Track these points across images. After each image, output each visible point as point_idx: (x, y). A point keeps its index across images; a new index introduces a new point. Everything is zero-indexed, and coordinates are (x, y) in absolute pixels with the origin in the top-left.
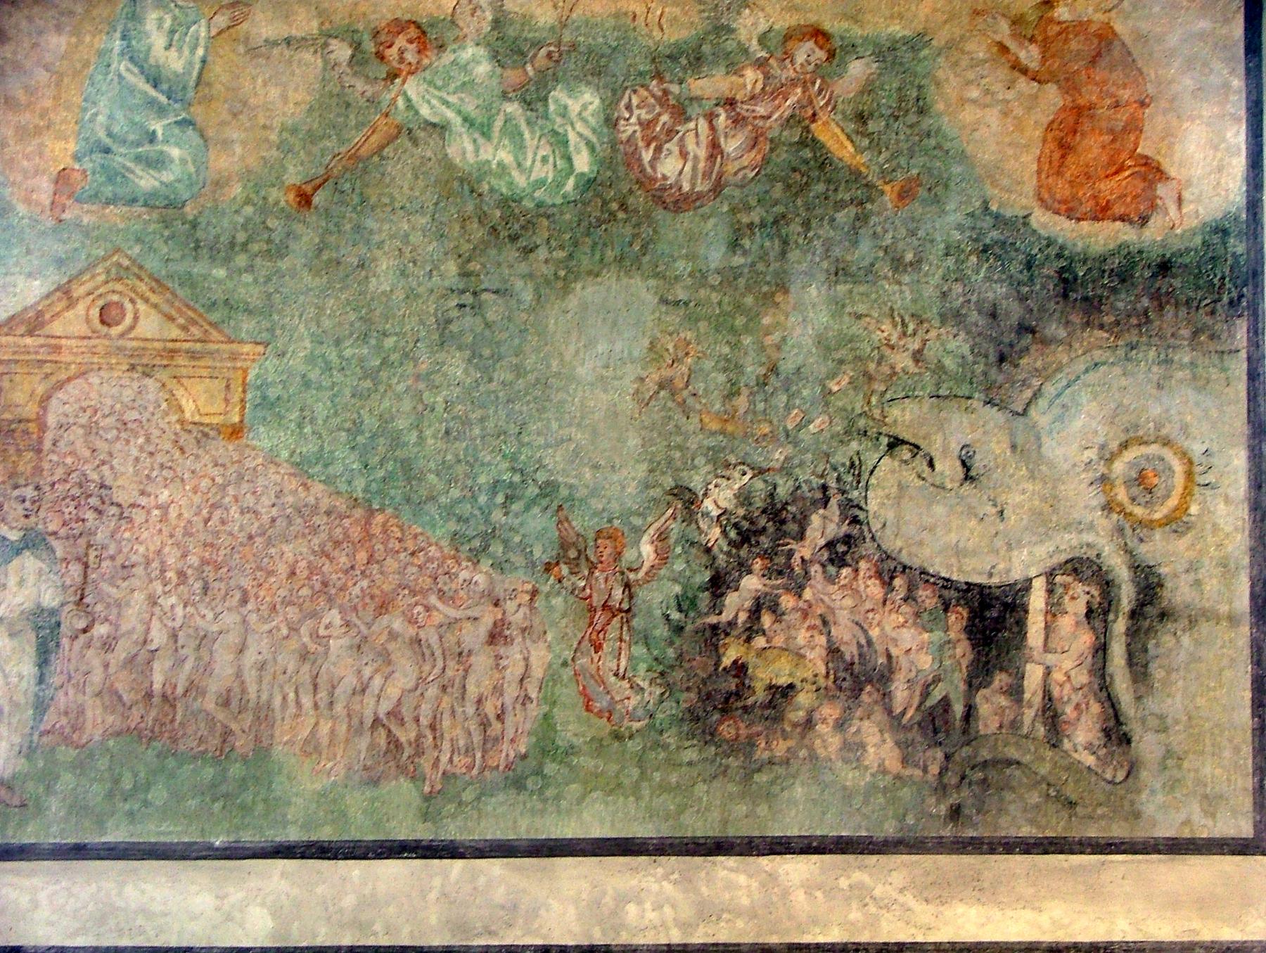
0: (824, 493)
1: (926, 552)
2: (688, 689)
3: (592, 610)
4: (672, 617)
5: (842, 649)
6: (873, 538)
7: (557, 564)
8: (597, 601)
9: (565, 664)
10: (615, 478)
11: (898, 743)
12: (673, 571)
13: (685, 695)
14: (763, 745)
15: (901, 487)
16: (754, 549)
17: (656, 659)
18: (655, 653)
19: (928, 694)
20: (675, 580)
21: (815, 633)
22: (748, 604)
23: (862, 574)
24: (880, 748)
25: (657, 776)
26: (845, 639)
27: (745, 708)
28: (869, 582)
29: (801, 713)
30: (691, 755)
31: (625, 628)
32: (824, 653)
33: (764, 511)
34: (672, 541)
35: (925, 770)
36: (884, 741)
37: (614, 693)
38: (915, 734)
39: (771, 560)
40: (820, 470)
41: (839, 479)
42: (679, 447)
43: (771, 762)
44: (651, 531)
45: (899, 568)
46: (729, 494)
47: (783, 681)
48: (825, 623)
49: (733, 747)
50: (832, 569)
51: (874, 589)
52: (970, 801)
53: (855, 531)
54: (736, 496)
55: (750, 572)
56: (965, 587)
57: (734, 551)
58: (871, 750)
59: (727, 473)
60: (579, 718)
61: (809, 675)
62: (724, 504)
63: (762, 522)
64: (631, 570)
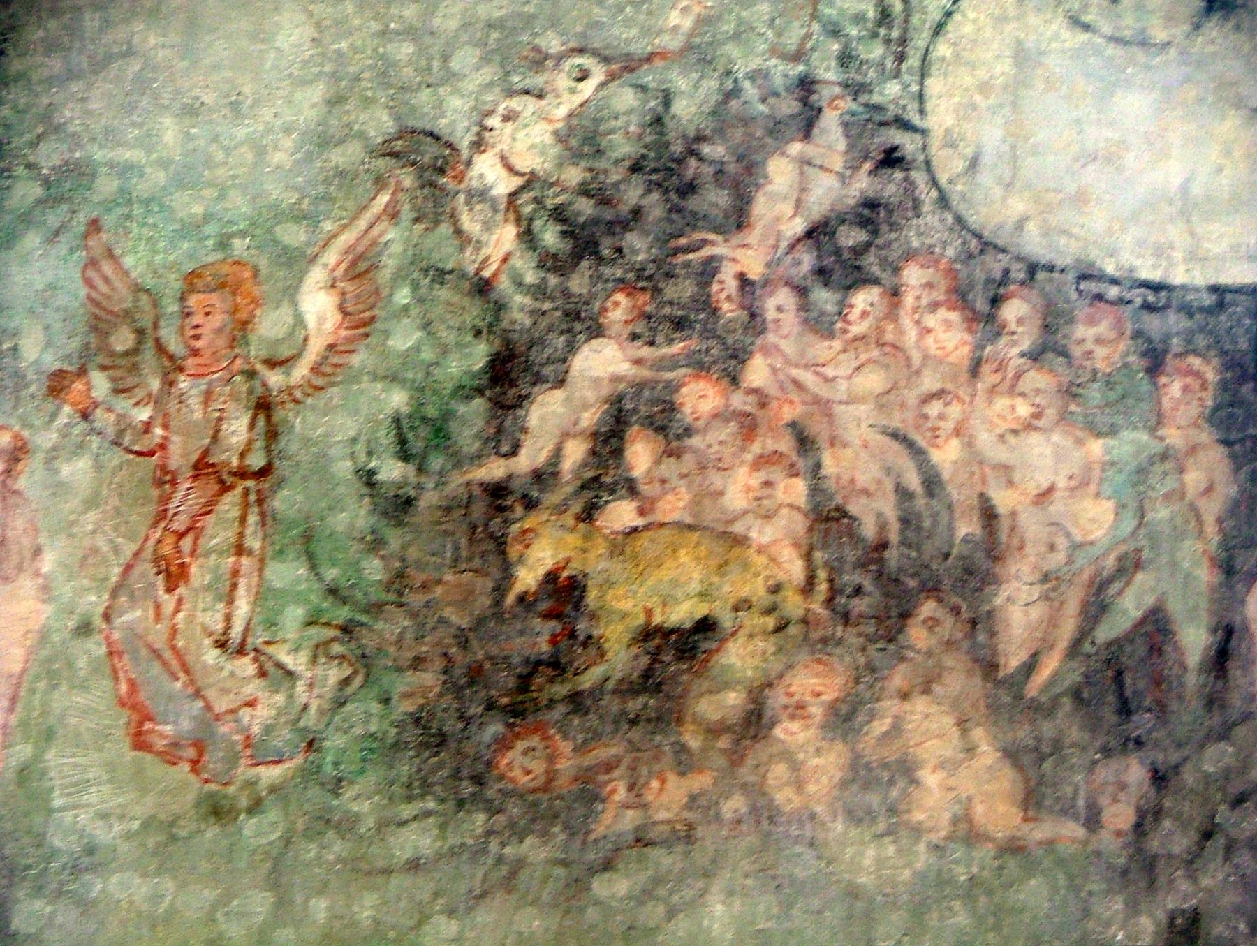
0: (805, 102)
1: (1096, 221)
2: (418, 663)
3: (166, 479)
4: (381, 477)
5: (853, 509)
6: (943, 201)
7: (82, 372)
8: (180, 455)
9: (84, 629)
10: (241, 133)
11: (1011, 754)
12: (385, 354)
13: (412, 679)
14: (621, 794)
15: (1022, 57)
16: (607, 271)
17: (333, 591)
18: (331, 574)
19: (1104, 608)
20: (393, 378)
21: (777, 474)
22: (588, 419)
23: (909, 300)
24: (955, 769)
25: (320, 908)
26: (863, 480)
27: (577, 701)
28: (931, 321)
29: (734, 699)
30: (417, 840)
31: (253, 519)
32: (800, 524)
33: (636, 168)
34: (384, 275)
35: (1093, 821)
36: (970, 750)
37: (211, 694)
38: (1067, 725)
39: (657, 291)
40: (791, 41)
41: (845, 59)
42: (410, 33)
43: (642, 840)
44: (331, 257)
45: (1018, 273)
46: (541, 133)
47: (682, 613)
48: (804, 442)
49: (545, 809)
50: (824, 297)
51: (948, 336)
52: (1231, 898)
53: (890, 187)
54: (560, 138)
55: (597, 332)
56: (1208, 300)
57: (553, 280)
58: (931, 779)
59: (538, 80)
60: (111, 767)
61: (756, 589)
62: (526, 162)
63: (633, 194)
64: (272, 364)
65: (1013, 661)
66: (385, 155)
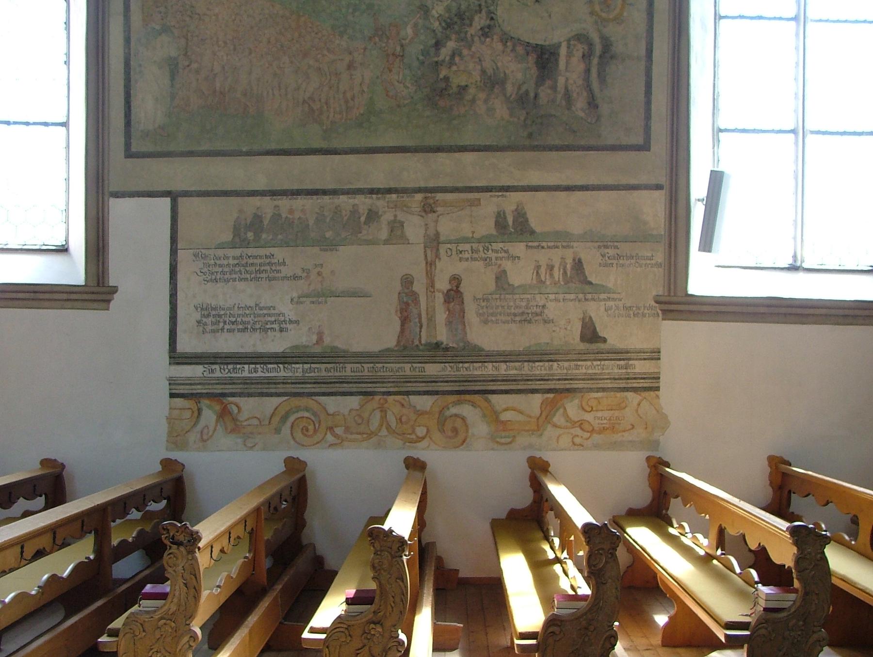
3: (388, 55)
9: (378, 78)
11: (508, 109)
24: (501, 110)
27: (449, 95)
30: (427, 113)
35: (519, 119)
43: (459, 116)
47: (463, 84)
50: (483, 39)
51: (500, 46)
53: (492, 23)
55: (451, 40)
62: (440, 12)
63: (455, 19)
65: (508, 95)
66: (590, 283)
